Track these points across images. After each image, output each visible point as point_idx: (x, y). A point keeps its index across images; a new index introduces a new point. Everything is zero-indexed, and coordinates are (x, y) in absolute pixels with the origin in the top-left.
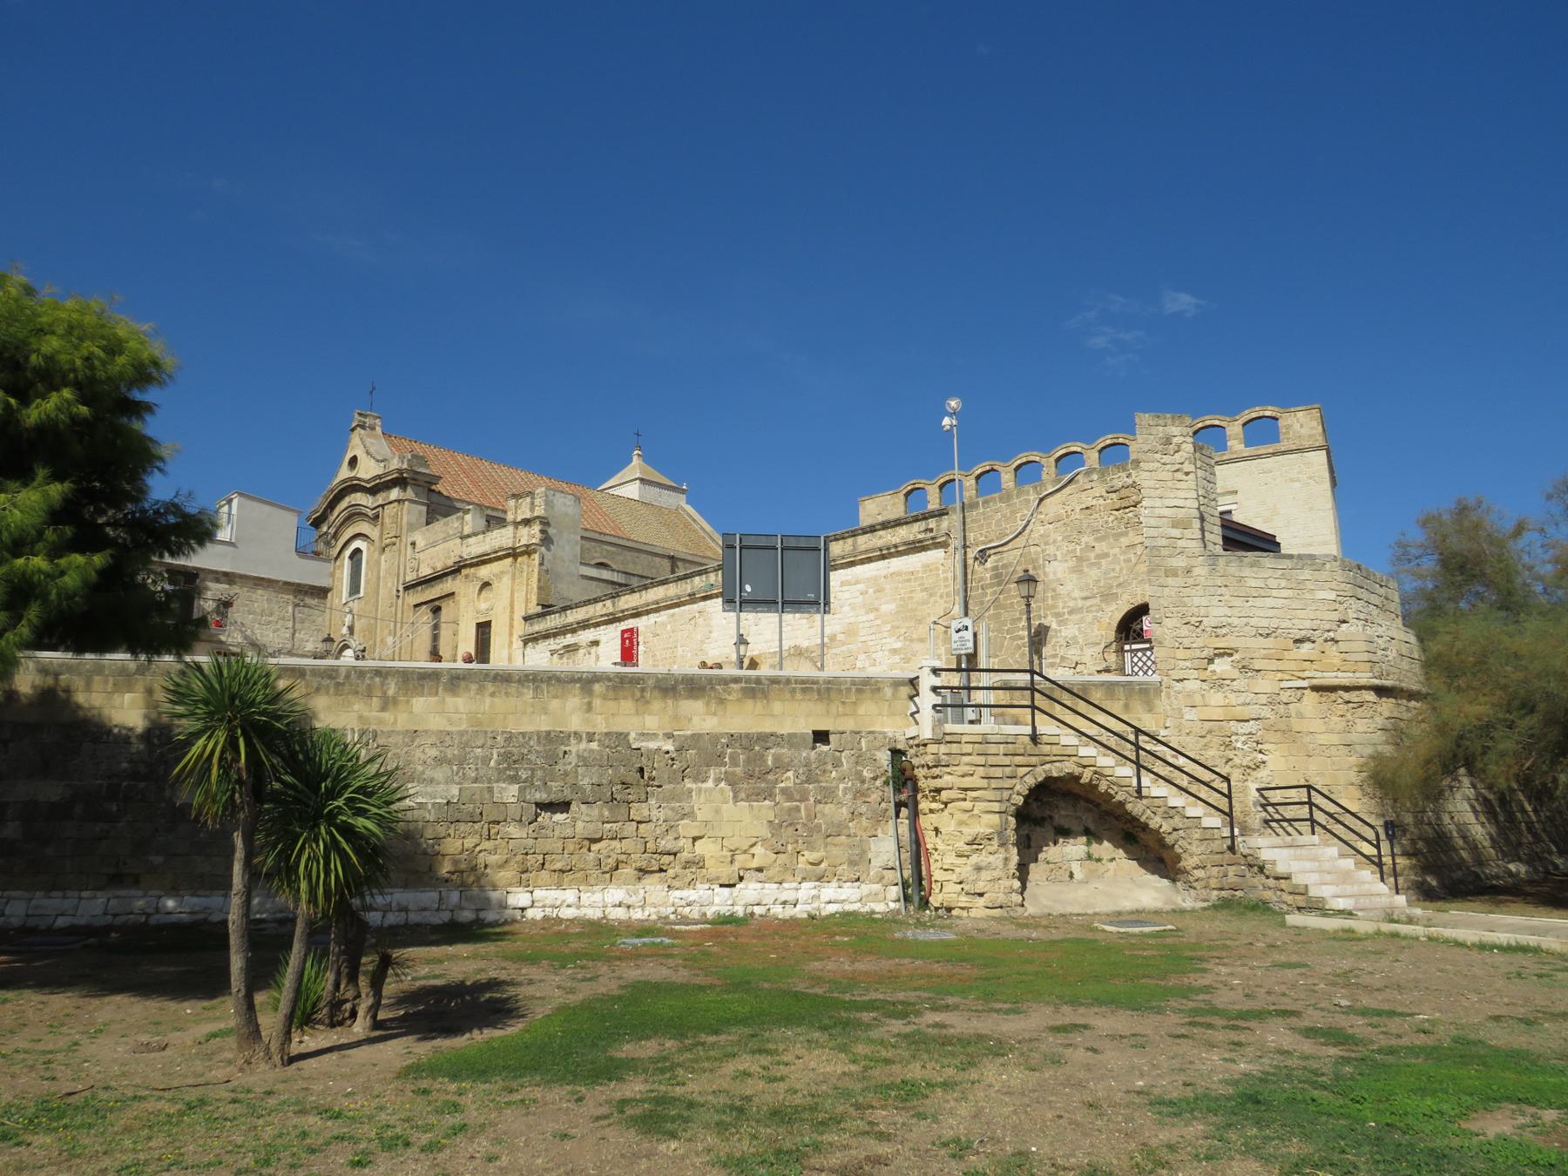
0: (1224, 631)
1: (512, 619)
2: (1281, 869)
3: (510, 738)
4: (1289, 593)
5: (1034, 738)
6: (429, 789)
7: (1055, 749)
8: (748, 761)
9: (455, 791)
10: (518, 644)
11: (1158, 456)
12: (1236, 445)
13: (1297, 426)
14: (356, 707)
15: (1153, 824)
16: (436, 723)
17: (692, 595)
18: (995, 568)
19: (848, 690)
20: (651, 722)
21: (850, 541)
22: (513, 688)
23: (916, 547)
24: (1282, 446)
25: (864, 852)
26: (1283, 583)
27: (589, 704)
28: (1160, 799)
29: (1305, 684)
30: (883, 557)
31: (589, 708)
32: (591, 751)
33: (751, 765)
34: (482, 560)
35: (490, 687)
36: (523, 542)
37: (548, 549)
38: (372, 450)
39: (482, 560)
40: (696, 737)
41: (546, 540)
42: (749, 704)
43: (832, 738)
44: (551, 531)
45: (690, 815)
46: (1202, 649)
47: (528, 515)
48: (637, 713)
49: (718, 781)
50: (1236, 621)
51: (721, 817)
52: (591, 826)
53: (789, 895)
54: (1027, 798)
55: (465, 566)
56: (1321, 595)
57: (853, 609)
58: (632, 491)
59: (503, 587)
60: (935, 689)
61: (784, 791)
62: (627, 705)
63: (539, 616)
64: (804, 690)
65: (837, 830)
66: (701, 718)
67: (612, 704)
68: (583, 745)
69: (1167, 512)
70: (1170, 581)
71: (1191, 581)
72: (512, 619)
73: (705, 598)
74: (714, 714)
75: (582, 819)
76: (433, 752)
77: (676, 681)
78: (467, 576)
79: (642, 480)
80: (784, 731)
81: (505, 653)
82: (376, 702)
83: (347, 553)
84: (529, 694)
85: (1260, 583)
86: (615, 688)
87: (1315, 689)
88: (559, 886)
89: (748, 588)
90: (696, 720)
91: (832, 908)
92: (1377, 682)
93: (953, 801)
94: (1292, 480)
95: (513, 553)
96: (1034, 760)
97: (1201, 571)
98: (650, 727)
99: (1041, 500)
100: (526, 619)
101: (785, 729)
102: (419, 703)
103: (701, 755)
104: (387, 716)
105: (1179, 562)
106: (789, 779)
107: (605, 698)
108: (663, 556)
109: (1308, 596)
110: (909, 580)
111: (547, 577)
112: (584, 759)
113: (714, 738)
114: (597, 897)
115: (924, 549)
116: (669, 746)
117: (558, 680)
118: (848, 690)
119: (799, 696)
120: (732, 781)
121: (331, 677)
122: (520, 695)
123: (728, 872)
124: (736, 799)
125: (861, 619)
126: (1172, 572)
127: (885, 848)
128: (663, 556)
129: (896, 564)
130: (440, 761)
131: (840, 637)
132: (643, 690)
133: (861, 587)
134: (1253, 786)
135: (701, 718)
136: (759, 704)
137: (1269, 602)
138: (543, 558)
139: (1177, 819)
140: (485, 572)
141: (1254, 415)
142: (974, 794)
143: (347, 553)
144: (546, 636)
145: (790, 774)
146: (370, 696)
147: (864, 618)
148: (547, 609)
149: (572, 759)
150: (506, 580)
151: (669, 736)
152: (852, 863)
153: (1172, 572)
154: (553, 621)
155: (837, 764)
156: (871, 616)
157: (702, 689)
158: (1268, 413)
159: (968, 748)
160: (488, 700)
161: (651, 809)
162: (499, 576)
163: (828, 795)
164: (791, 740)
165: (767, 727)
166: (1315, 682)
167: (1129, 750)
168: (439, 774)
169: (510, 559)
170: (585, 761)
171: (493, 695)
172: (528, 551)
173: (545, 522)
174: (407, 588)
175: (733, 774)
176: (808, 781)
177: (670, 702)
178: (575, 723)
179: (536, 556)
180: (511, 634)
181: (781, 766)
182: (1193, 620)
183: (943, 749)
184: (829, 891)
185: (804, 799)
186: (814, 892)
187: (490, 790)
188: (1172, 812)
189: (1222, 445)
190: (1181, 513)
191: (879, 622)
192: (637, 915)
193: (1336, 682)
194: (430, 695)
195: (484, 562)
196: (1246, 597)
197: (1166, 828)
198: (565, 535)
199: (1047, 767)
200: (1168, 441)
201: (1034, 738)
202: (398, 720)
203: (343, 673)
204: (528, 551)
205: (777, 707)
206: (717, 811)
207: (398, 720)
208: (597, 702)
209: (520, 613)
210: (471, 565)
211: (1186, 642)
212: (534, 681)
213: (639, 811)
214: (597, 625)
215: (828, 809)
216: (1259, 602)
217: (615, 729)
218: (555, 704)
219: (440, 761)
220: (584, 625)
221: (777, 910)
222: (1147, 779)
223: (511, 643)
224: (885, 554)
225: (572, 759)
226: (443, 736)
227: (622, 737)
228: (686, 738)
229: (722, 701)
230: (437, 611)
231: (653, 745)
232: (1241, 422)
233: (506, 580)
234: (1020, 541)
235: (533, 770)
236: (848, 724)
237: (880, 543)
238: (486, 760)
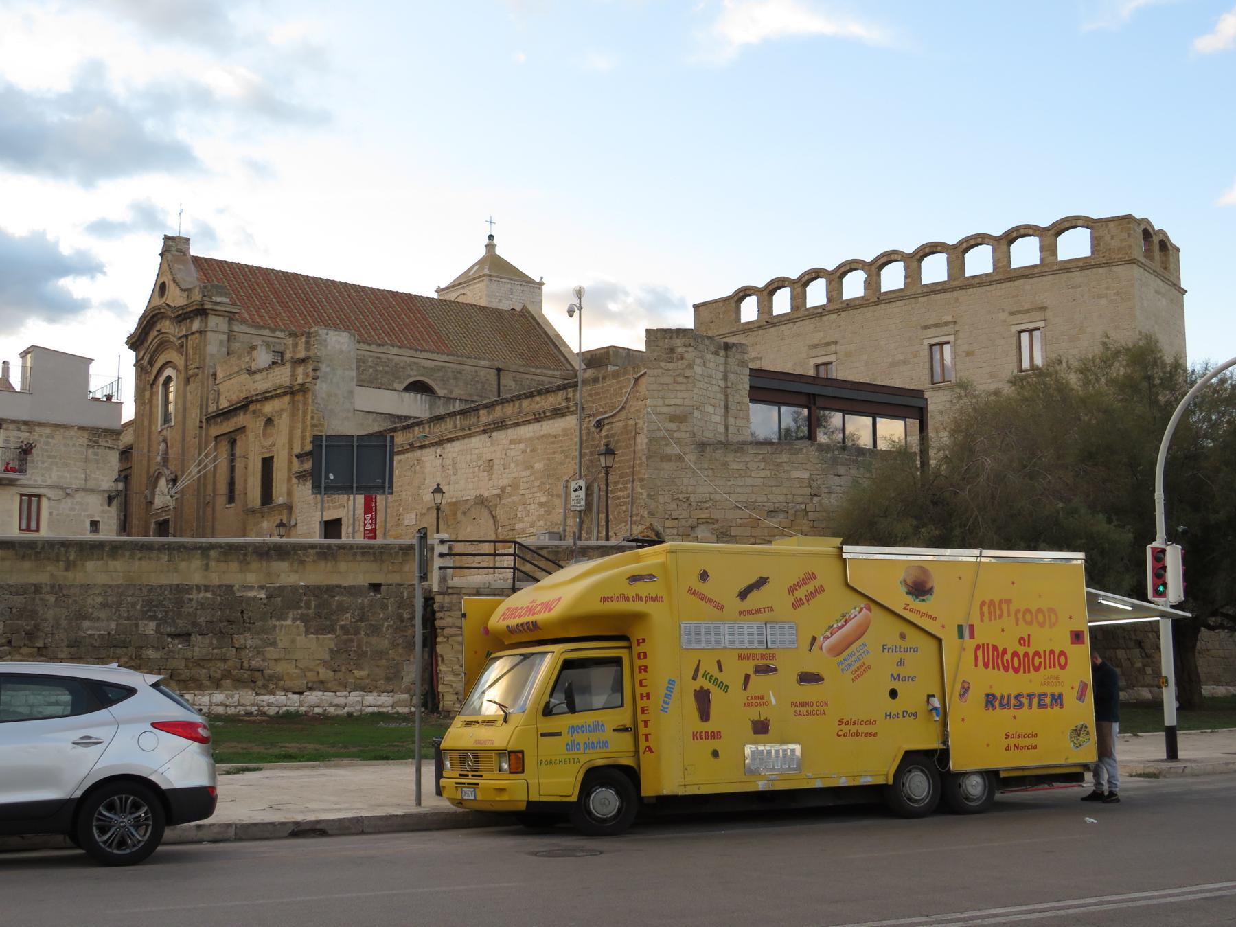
0: (707, 505)
3: (151, 589)
4: (768, 473)
6: (96, 625)
8: (318, 606)
9: (113, 625)
11: (662, 364)
13: (1108, 237)
14: (49, 568)
16: (102, 579)
17: (411, 445)
18: (607, 436)
19: (397, 553)
20: (251, 578)
21: (517, 404)
22: (154, 554)
23: (558, 413)
25: (398, 671)
26: (762, 465)
27: (207, 565)
30: (537, 420)
31: (207, 567)
32: (207, 598)
33: (320, 608)
34: (266, 397)
35: (138, 554)
36: (300, 381)
38: (178, 277)
40: (282, 588)
42: (322, 564)
45: (274, 644)
46: (687, 520)
48: (241, 571)
49: (294, 620)
51: (298, 644)
52: (204, 651)
53: (341, 701)
55: (252, 402)
56: (795, 474)
57: (517, 465)
61: (342, 627)
62: (234, 566)
64: (363, 554)
65: (380, 654)
66: (287, 575)
67: (223, 566)
68: (202, 595)
69: (665, 410)
70: (666, 465)
73: (422, 447)
74: (297, 572)
75: (201, 646)
76: (99, 599)
77: (269, 549)
78: (254, 412)
80: (346, 584)
81: (284, 489)
82: (62, 565)
83: (162, 379)
84: (165, 558)
86: (225, 554)
89: (331, 476)
90: (283, 575)
91: (370, 710)
94: (1100, 297)
97: (690, 458)
98: (250, 580)
99: (637, 380)
101: (348, 581)
102: (90, 565)
103: (284, 600)
104: (70, 574)
105: (675, 450)
106: (346, 619)
107: (218, 561)
109: (783, 476)
110: (553, 443)
112: (202, 604)
113: (295, 589)
115: (563, 415)
116: (262, 595)
117: (185, 547)
118: (397, 553)
119: (359, 558)
120: (304, 619)
121: (32, 548)
122: (159, 559)
123: (300, 683)
124: (307, 632)
126: (668, 459)
127: (412, 672)
130: (104, 605)
132: (245, 555)
133: (522, 446)
135: (287, 575)
136: (329, 564)
137: (749, 481)
140: (268, 408)
143: (162, 379)
145: (348, 615)
146: (58, 561)
149: (194, 604)
151: (262, 587)
152: (388, 679)
153: (668, 459)
155: (384, 607)
156: (528, 473)
157: (288, 553)
160: (137, 563)
161: (246, 640)
163: (375, 630)
164: (351, 591)
165: (335, 580)
168: (102, 615)
169: (287, 398)
170: (202, 605)
171: (140, 559)
174: (208, 420)
175: (307, 615)
176: (361, 620)
177: (264, 563)
178: (197, 578)
181: (342, 609)
182: (681, 496)
183: (447, 599)
184: (370, 699)
185: (357, 633)
186: (359, 699)
187: (137, 625)
191: (532, 478)
192: (231, 711)
194: (98, 559)
195: (267, 399)
196: (728, 478)
198: (339, 372)
200: (672, 350)
202: (76, 577)
203: (40, 546)
205: (343, 566)
206: (293, 641)
207: (76, 577)
208: (213, 564)
210: (257, 401)
211: (675, 514)
212: (168, 549)
213: (240, 640)
215: (374, 640)
216: (739, 482)
217: (228, 582)
218: (183, 565)
219: (104, 605)
221: (332, 710)
224: (538, 418)
225: (194, 604)
226: (105, 587)
227: (230, 588)
228: (275, 588)
229: (302, 562)
230: (233, 443)
231: (251, 594)
233: (285, 416)
234: (623, 415)
236: (395, 579)
238: (134, 605)
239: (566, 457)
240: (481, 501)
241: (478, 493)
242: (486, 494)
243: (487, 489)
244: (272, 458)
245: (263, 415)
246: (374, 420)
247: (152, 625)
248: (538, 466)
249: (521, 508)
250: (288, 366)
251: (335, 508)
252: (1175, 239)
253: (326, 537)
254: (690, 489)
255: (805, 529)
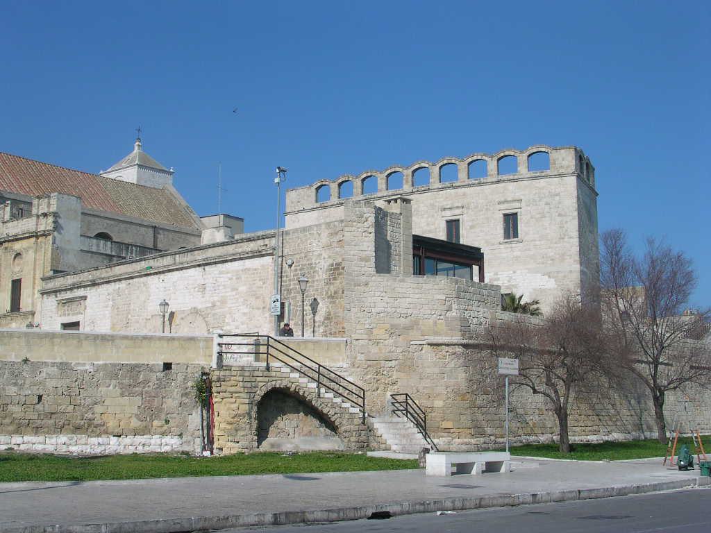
1: (34, 278)
2: (379, 433)
5: (268, 368)
7: (278, 374)
10: (37, 295)
12: (523, 169)
15: (325, 411)
23: (258, 254)
24: (549, 172)
25: (185, 422)
28: (327, 400)
29: (424, 342)
30: (241, 259)
34: (16, 239)
37: (60, 233)
39: (16, 239)
41: (57, 227)
43: (173, 366)
44: (61, 221)
47: (46, 211)
50: (389, 310)
54: (263, 397)
58: (130, 175)
59: (29, 256)
60: (219, 344)
63: (50, 278)
71: (367, 289)
72: (34, 278)
78: (6, 248)
79: (139, 166)
81: (30, 300)
85: (404, 291)
87: (431, 345)
88: (36, 434)
92: (465, 341)
93: (226, 398)
95: (36, 235)
96: (267, 379)
100: (43, 279)
105: (363, 279)
108: (147, 226)
111: (57, 252)
114: (53, 440)
125: (228, 294)
128: (147, 226)
129: (248, 263)
131: (218, 304)
133: (229, 275)
134: (389, 394)
138: (54, 239)
139: (337, 409)
140: (18, 246)
141: (535, 150)
142: (237, 395)
144: (56, 292)
147: (230, 294)
148: (57, 272)
150: (31, 252)
154: (59, 282)
156: (234, 293)
158: (543, 150)
159: (234, 373)
162: (27, 250)
166: (430, 341)
167: (316, 376)
172: (45, 235)
173: (56, 215)
179: (50, 238)
180: (34, 288)
188: (334, 405)
189: (514, 169)
190: (363, 254)
193: (440, 341)
195: (17, 240)
197: (332, 413)
199: (274, 383)
201: (268, 368)
204: (45, 235)
209: (39, 275)
210: (9, 241)
211: (362, 321)
214: (85, 287)
220: (78, 286)
222: (323, 390)
223: (34, 294)
225: (44, 374)
232: (527, 154)
233: (31, 252)
235: (25, 380)
237: (240, 250)
239: (264, 283)
240: (196, 311)
241: (193, 306)
242: (200, 307)
243: (201, 303)
244: (20, 281)
245: (13, 250)
246: (91, 257)
247: (15, 389)
248: (243, 289)
249: (228, 316)
250: (35, 218)
251: (73, 314)
252: (593, 163)
253: (64, 329)
254: (372, 305)
255: (82, 336)
